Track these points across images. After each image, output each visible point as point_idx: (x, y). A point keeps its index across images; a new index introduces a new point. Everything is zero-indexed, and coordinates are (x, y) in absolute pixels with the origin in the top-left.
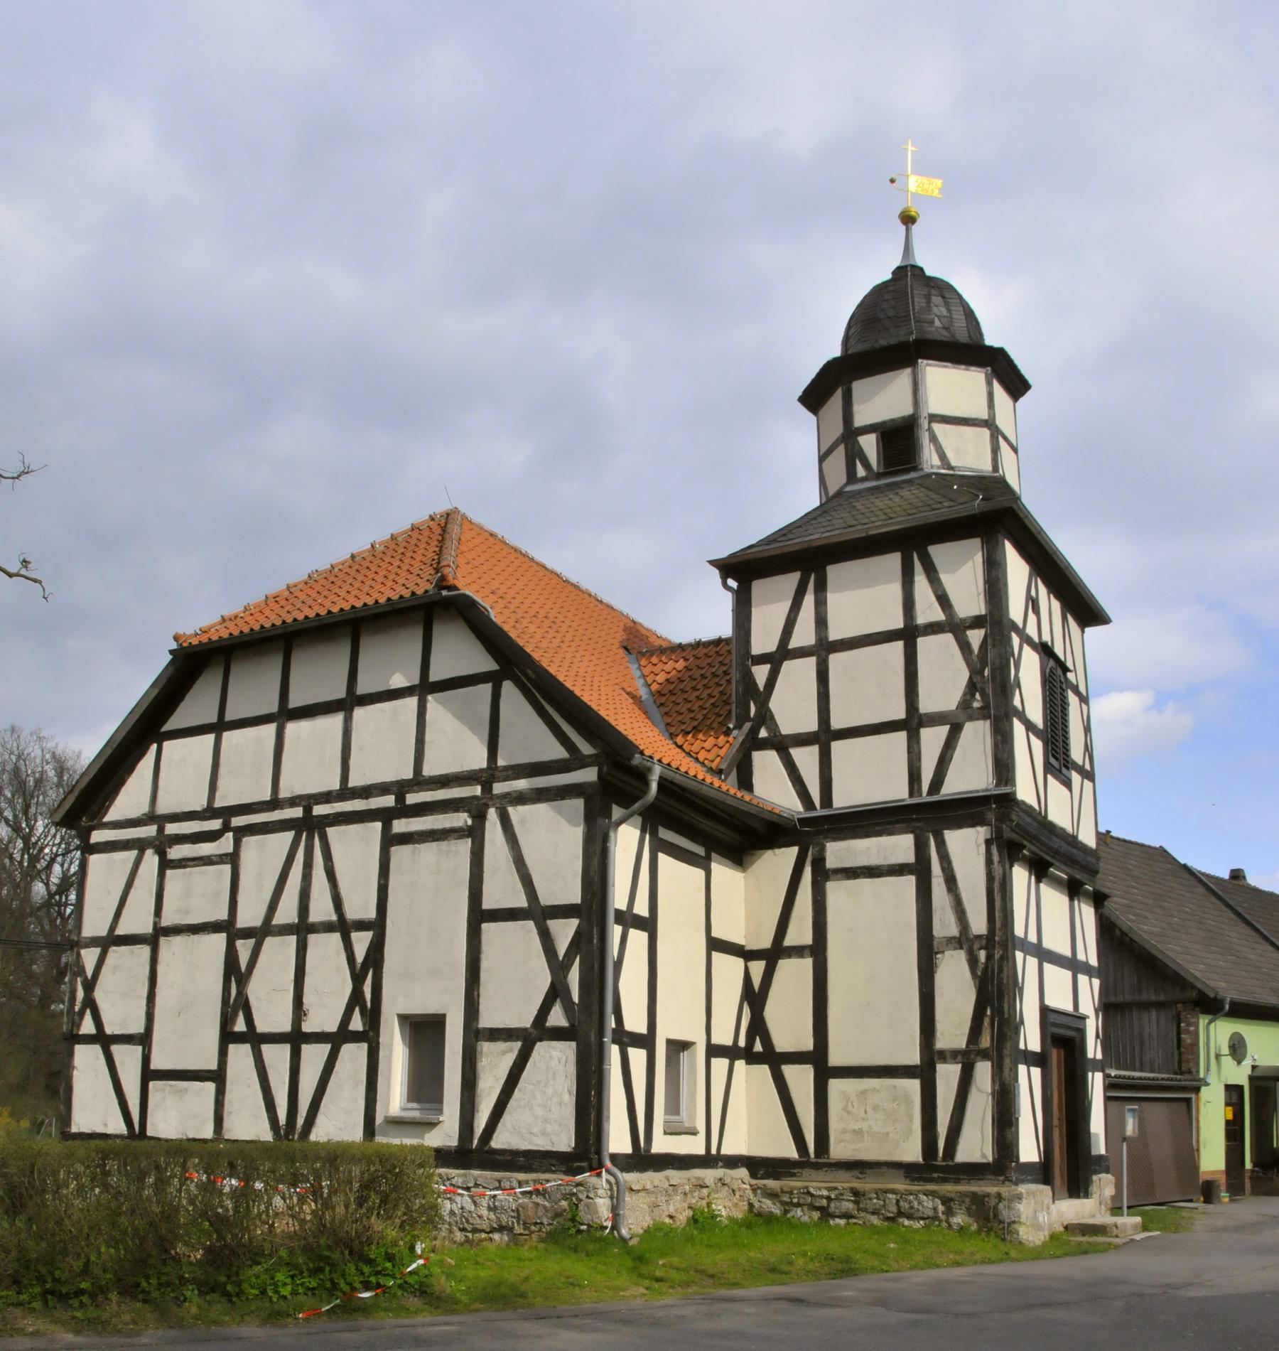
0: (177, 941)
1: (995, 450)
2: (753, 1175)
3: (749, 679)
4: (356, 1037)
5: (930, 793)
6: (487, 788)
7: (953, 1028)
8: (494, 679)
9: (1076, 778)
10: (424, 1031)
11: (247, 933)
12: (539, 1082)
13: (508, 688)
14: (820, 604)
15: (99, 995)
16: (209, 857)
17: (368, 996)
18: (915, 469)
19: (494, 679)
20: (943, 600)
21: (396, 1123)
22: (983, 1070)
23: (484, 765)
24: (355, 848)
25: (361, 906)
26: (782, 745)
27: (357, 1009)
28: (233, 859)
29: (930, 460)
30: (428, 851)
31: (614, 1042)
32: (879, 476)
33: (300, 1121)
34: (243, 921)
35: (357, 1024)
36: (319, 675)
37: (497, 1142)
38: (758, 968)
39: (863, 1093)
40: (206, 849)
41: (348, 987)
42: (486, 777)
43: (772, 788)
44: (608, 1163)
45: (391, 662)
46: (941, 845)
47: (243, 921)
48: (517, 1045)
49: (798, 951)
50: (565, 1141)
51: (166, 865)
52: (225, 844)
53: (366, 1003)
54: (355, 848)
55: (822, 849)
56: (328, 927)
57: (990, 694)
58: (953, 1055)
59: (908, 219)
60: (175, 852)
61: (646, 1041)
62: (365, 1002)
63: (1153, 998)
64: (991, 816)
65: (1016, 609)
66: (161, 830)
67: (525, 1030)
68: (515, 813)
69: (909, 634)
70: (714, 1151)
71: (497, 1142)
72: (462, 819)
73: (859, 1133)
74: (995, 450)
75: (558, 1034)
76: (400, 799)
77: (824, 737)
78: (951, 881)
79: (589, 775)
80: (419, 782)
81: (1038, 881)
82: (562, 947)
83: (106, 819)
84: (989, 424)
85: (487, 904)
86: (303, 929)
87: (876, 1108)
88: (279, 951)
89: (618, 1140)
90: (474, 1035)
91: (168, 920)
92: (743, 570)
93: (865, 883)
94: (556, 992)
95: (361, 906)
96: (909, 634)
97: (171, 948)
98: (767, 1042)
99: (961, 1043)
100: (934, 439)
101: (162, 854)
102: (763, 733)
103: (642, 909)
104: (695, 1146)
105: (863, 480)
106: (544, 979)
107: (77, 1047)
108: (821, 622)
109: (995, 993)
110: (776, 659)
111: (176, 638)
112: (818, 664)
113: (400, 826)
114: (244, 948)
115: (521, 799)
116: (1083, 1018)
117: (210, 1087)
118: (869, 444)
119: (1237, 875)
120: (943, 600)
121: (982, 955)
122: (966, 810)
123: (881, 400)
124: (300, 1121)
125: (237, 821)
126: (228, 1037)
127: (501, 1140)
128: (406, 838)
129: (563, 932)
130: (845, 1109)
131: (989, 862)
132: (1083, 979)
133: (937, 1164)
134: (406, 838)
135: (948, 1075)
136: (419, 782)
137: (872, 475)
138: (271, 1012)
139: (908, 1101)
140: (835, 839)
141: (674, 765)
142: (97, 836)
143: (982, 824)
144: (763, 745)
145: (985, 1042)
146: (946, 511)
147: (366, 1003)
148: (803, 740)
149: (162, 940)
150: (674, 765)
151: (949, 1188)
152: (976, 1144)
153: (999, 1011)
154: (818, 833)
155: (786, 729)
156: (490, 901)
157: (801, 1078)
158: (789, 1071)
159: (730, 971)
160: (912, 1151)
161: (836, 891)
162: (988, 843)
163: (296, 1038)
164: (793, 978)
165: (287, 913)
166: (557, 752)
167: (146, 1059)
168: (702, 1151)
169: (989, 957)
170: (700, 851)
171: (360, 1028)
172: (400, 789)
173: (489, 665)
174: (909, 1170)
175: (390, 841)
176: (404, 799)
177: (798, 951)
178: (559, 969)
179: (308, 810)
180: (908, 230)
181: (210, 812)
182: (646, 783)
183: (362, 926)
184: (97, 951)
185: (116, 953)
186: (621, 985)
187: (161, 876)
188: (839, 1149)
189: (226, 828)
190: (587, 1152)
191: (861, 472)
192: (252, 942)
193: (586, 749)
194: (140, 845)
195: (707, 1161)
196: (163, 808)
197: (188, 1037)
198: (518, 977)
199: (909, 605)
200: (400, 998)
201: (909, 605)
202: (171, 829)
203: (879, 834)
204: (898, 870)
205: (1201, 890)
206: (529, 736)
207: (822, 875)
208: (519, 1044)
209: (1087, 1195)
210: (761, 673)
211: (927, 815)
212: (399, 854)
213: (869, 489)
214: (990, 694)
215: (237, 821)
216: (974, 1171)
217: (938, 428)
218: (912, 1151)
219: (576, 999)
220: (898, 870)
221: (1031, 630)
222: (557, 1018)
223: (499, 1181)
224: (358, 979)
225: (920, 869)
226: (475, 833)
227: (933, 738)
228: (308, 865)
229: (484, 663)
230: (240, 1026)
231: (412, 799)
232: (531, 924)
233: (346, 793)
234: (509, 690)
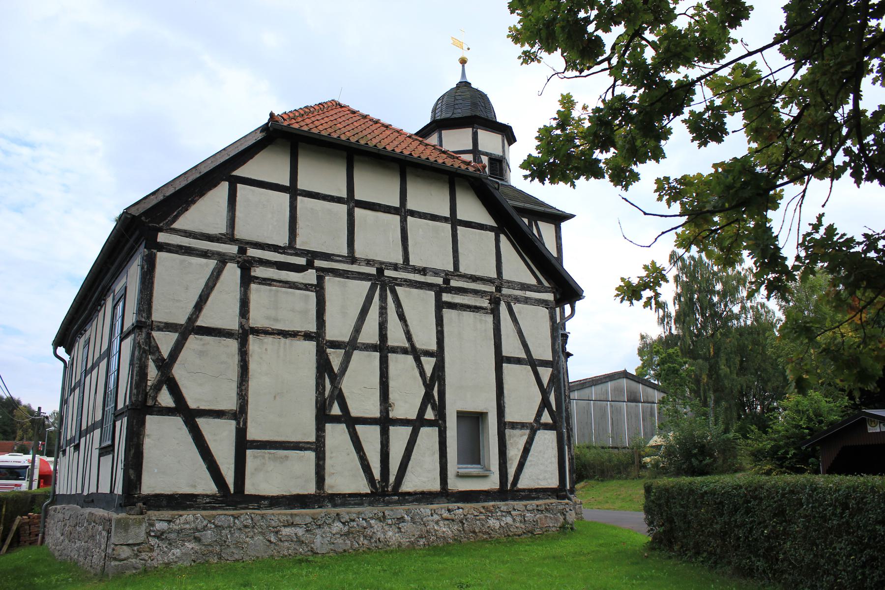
4: (430, 423)
19: (234, 182)
27: (429, 407)
33: (392, 479)
35: (430, 415)
37: (521, 485)
41: (422, 391)
47: (331, 334)
51: (247, 280)
52: (310, 277)
54: (419, 305)
59: (463, 62)
60: (259, 272)
62: (434, 400)
67: (531, 423)
71: (521, 485)
75: (546, 427)
82: (545, 381)
90: (502, 425)
94: (545, 403)
107: (149, 418)
124: (392, 479)
126: (323, 417)
127: (523, 484)
128: (452, 306)
138: (362, 400)
175: (440, 306)
176: (308, 261)
179: (380, 271)
180: (463, 66)
189: (310, 265)
192: (175, 336)
215: (318, 263)
219: (554, 409)
222: (546, 418)
223: (526, 506)
224: (429, 387)
230: (336, 410)
232: (356, 352)
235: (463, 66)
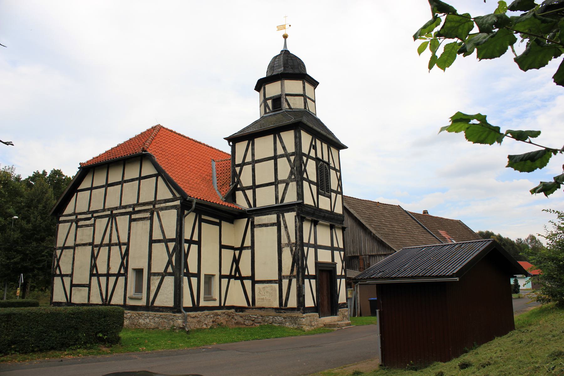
0: (80, 248)
1: (305, 102)
2: (236, 311)
3: (234, 171)
6: (154, 206)
7: (286, 271)
8: (156, 176)
9: (333, 195)
10: (139, 272)
11: (96, 246)
14: (282, 142)
15: (60, 263)
18: (281, 110)
19: (156, 176)
20: (284, 148)
21: (131, 298)
22: (294, 281)
23: (153, 200)
24: (123, 222)
25: (124, 239)
26: (243, 189)
28: (94, 225)
29: (285, 106)
30: (140, 223)
31: (185, 276)
32: (272, 112)
33: (108, 298)
34: (96, 243)
35: (122, 271)
36: (115, 176)
37: (156, 304)
38: (237, 253)
39: (264, 288)
40: (88, 222)
42: (154, 203)
43: (241, 202)
44: (183, 310)
45: (132, 172)
46: (283, 217)
47: (96, 243)
49: (247, 248)
50: (171, 304)
51: (77, 227)
53: (124, 266)
54: (123, 222)
55: (253, 219)
56: (116, 244)
57: (298, 174)
59: (285, 37)
60: (80, 223)
61: (198, 275)
63: (383, 253)
64: (296, 209)
65: (305, 149)
66: (76, 217)
68: (161, 213)
69: (275, 158)
70: (222, 305)
71: (156, 304)
72: (148, 215)
73: (263, 299)
74: (305, 102)
75: (170, 274)
76: (134, 209)
77: (254, 187)
78: (286, 227)
79: (178, 203)
80: (138, 204)
81: (315, 226)
84: (304, 95)
85: (154, 238)
86: (110, 245)
87: (267, 292)
88: (104, 251)
89: (187, 302)
90: (150, 274)
91: (78, 242)
92: (234, 140)
93: (264, 228)
94: (170, 262)
95: (124, 239)
96: (275, 158)
97: (78, 249)
98: (240, 274)
99: (288, 273)
100: (287, 101)
101: (77, 223)
102: (239, 186)
103: (195, 238)
104: (217, 304)
105: (269, 113)
107: (55, 278)
108: (253, 155)
109: (299, 260)
110: (244, 164)
111: (80, 164)
113: (133, 216)
114: (96, 250)
116: (336, 264)
117: (87, 289)
118: (270, 102)
119: (425, 212)
120: (284, 148)
121: (294, 248)
122: (289, 207)
123: (273, 89)
125: (95, 215)
126: (92, 275)
128: (135, 220)
129: (172, 245)
132: (336, 253)
133: (282, 308)
134: (135, 220)
135: (285, 282)
136: (138, 204)
138: (102, 269)
139: (276, 290)
140: (257, 216)
141: (202, 199)
143: (294, 211)
144: (239, 190)
146: (286, 122)
147: (124, 266)
148: (249, 188)
150: (202, 199)
151: (285, 315)
152: (293, 302)
154: (253, 214)
155: (244, 185)
157: (248, 283)
158: (245, 282)
159: (228, 255)
160: (276, 305)
161: (256, 230)
162: (295, 216)
163: (108, 275)
164: (246, 254)
165: (106, 241)
166: (170, 196)
167: (72, 281)
168: (218, 305)
169: (296, 249)
170: (218, 221)
172: (134, 206)
173: (156, 172)
174: (276, 309)
175: (131, 220)
177: (247, 248)
178: (170, 256)
179: (112, 212)
180: (285, 40)
181: (89, 212)
182: (192, 205)
183: (124, 244)
185: (65, 251)
186: (188, 260)
187: (76, 230)
188: (258, 304)
190: (177, 307)
191: (268, 111)
193: (178, 195)
194: (71, 221)
195: (220, 308)
196: (77, 211)
197: (82, 276)
200: (133, 264)
202: (79, 217)
204: (272, 225)
205: (410, 218)
206: (164, 193)
207: (253, 226)
209: (336, 315)
210: (238, 169)
211: (280, 209)
212: (133, 224)
213: (270, 115)
214: (298, 174)
215: (95, 215)
216: (292, 309)
217: (288, 98)
218: (276, 305)
220: (272, 225)
221: (312, 154)
222: (170, 270)
224: (123, 259)
225: (278, 224)
226: (151, 219)
227: (281, 187)
228: (112, 227)
229: (154, 172)
231: (136, 209)
233: (121, 207)
234: (160, 178)
235: (285, 40)
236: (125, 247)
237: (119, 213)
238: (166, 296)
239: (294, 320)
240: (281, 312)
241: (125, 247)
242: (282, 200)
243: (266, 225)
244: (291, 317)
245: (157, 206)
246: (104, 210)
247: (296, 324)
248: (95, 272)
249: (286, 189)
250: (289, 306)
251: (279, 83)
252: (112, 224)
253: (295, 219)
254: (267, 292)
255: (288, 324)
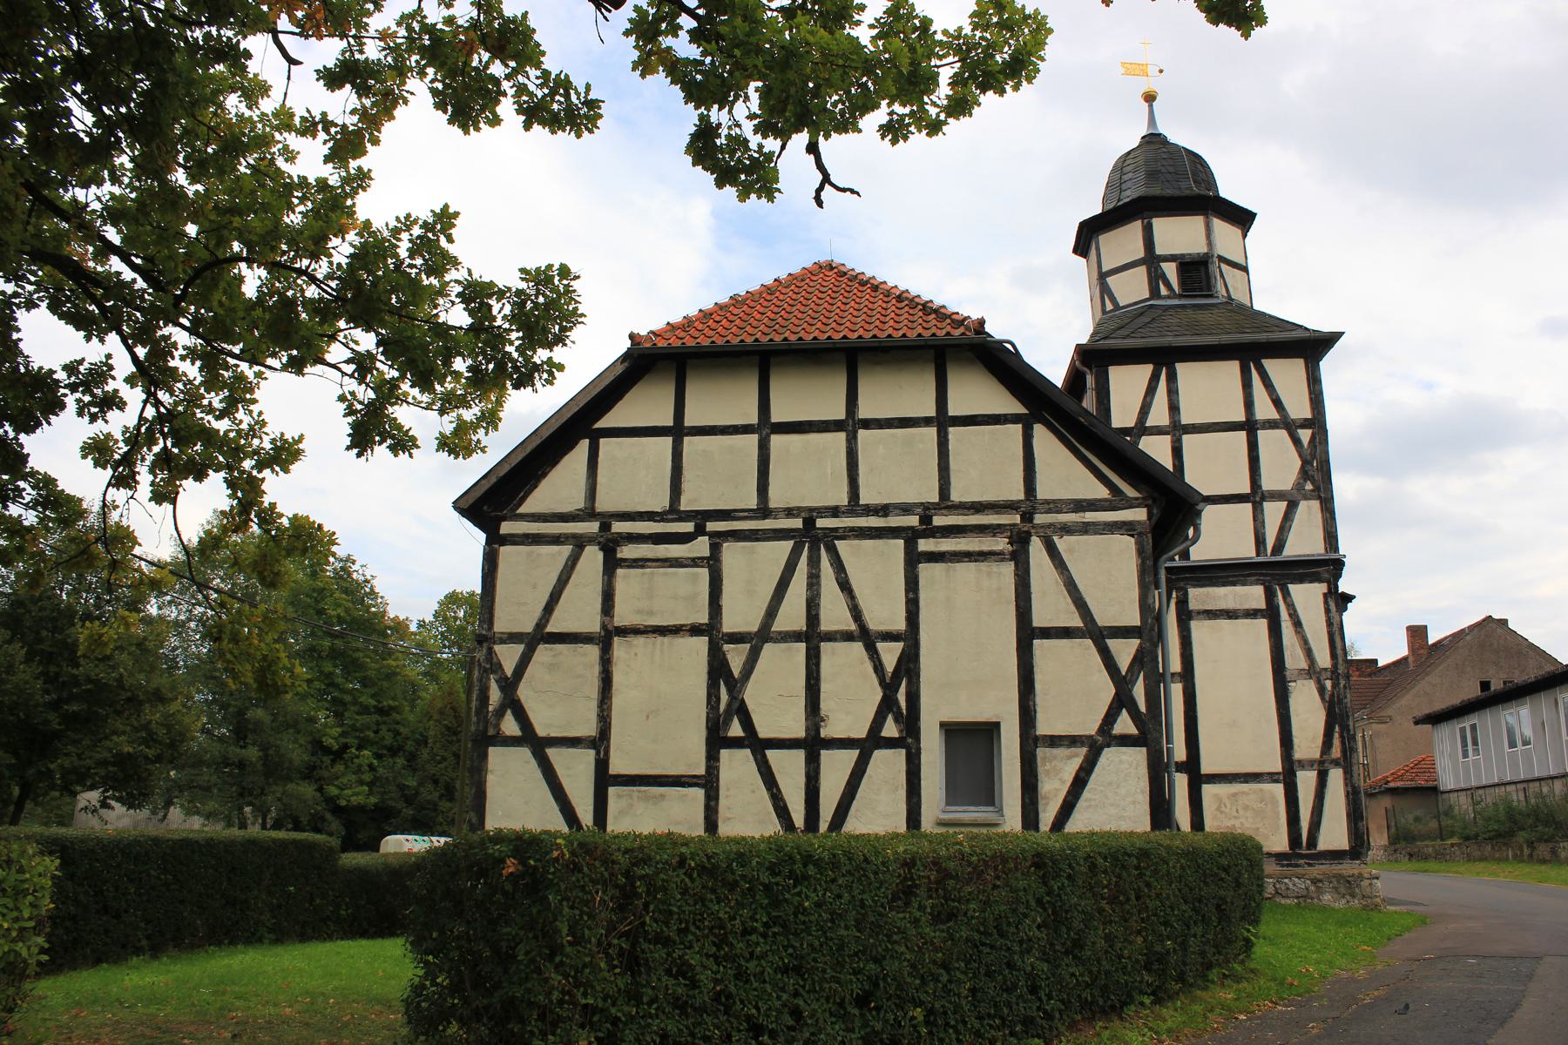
5: (1273, 554)
7: (1308, 741)
10: (975, 741)
12: (1110, 784)
13: (1039, 431)
14: (1173, 392)
16: (676, 559)
17: (903, 704)
18: (1211, 296)
20: (1277, 403)
22: (1336, 777)
25: (886, 613)
30: (966, 572)
32: (1180, 296)
34: (729, 624)
35: (890, 729)
39: (1235, 795)
46: (1286, 594)
47: (729, 624)
48: (1083, 751)
51: (612, 564)
52: (701, 546)
58: (1310, 764)
59: (1150, 98)
60: (627, 552)
62: (899, 708)
67: (1090, 737)
69: (1250, 426)
72: (1001, 544)
78: (1297, 624)
82: (1124, 663)
83: (521, 510)
90: (1030, 742)
93: (1224, 623)
94: (1122, 700)
106: (1108, 691)
108: (1174, 408)
112: (760, 441)
113: (924, 545)
114: (736, 657)
115: (1066, 530)
117: (699, 793)
118: (1170, 270)
120: (1277, 403)
121: (1328, 684)
126: (716, 740)
129: (1124, 651)
130: (1218, 809)
131: (1327, 611)
135: (1306, 781)
137: (1172, 295)
139: (1275, 802)
142: (506, 528)
143: (1320, 581)
145: (1336, 752)
149: (617, 641)
153: (1345, 728)
156: (1039, 619)
167: (602, 765)
169: (1333, 686)
171: (896, 735)
172: (926, 512)
175: (914, 559)
180: (1151, 106)
184: (519, 649)
189: (701, 530)
191: (1164, 291)
193: (1130, 492)
194: (580, 543)
198: (1075, 689)
199: (1249, 404)
201: (1249, 404)
203: (1234, 584)
204: (1252, 614)
208: (1085, 750)
212: (926, 571)
215: (712, 526)
216: (1336, 855)
220: (1252, 614)
222: (1125, 725)
224: (889, 687)
231: (938, 521)
235: (1151, 106)
236: (898, 647)
237: (852, 529)
238: (1113, 811)
239: (1349, 885)
240: (1297, 866)
241: (898, 647)
242: (1279, 546)
243: (1230, 614)
244: (1339, 877)
245: (1039, 519)
246: (764, 511)
247: (1353, 896)
248: (736, 730)
249: (1288, 517)
250: (1323, 844)
251: (1136, 227)
252: (814, 562)
253: (1326, 602)
254: (1246, 808)
255: (1327, 897)
